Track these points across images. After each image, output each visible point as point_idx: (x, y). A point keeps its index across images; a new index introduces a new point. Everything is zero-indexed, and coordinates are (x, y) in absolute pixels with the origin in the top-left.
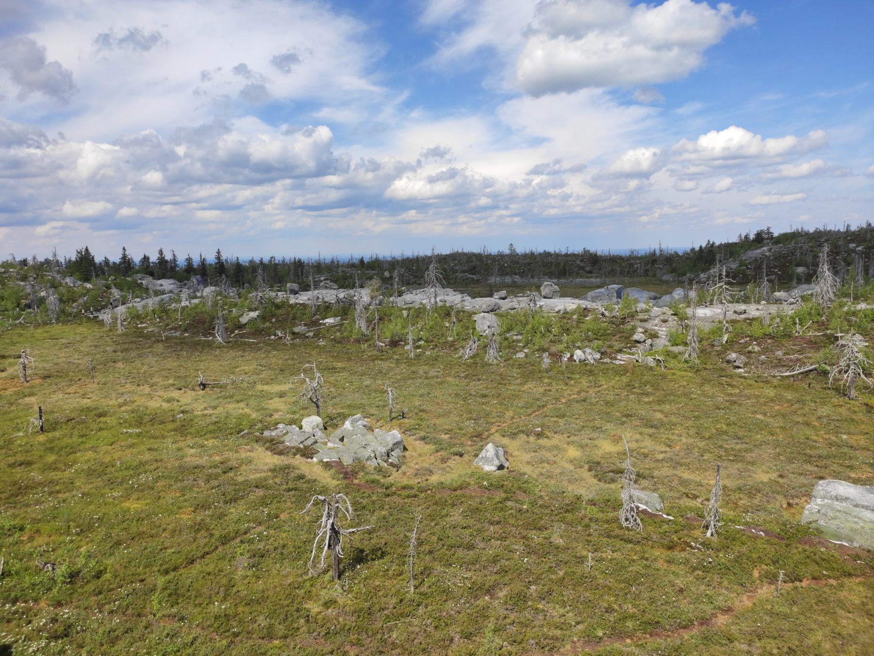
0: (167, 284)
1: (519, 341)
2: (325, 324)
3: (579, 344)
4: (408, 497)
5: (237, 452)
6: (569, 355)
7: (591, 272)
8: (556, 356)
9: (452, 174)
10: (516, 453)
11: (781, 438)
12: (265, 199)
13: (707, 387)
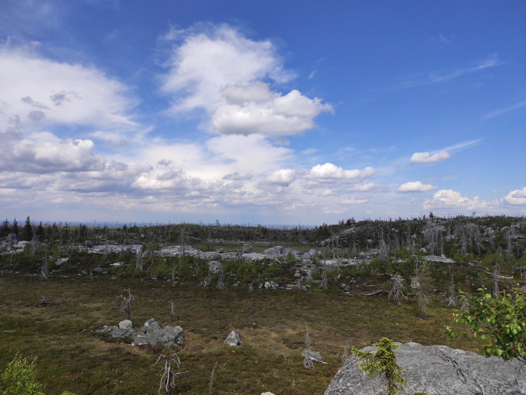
1: (234, 277)
2: (114, 266)
3: (266, 279)
4: (194, 360)
5: (83, 342)
6: (262, 285)
7: (263, 238)
8: (256, 285)
9: (173, 176)
10: (245, 336)
11: (370, 325)
12: (48, 183)
13: (333, 301)
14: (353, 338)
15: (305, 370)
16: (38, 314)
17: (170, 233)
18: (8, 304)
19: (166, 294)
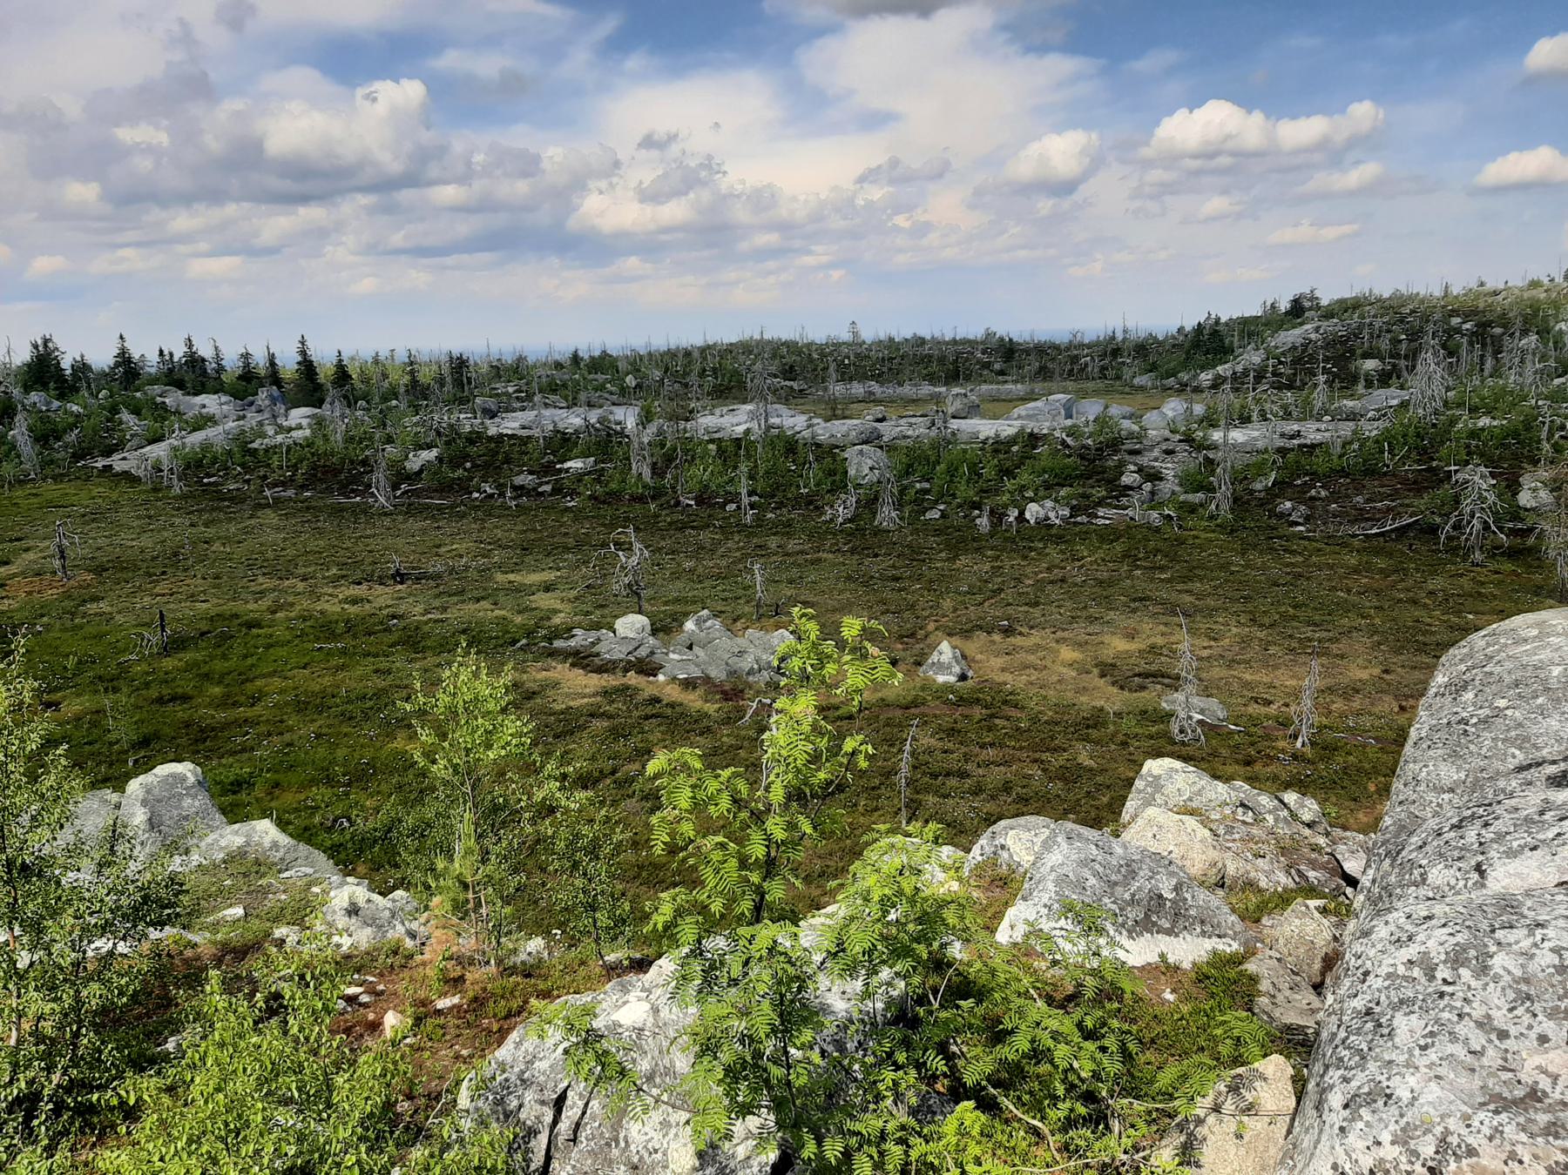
0: (211, 403)
1: (927, 491)
2: (567, 470)
3: (1030, 494)
7: (1002, 373)
8: (997, 516)
11: (1377, 621)
12: (321, 234)
14: (1324, 660)
15: (1177, 748)
16: (390, 602)
17: (721, 372)
18: (304, 579)
19: (730, 544)
